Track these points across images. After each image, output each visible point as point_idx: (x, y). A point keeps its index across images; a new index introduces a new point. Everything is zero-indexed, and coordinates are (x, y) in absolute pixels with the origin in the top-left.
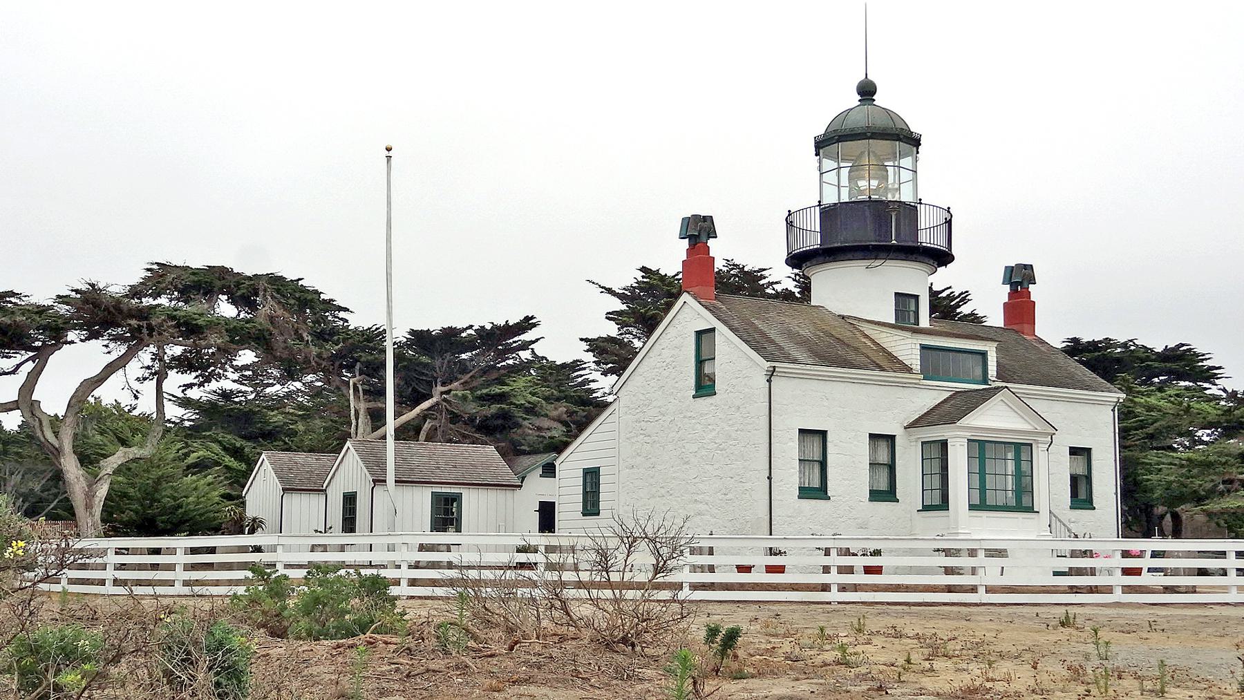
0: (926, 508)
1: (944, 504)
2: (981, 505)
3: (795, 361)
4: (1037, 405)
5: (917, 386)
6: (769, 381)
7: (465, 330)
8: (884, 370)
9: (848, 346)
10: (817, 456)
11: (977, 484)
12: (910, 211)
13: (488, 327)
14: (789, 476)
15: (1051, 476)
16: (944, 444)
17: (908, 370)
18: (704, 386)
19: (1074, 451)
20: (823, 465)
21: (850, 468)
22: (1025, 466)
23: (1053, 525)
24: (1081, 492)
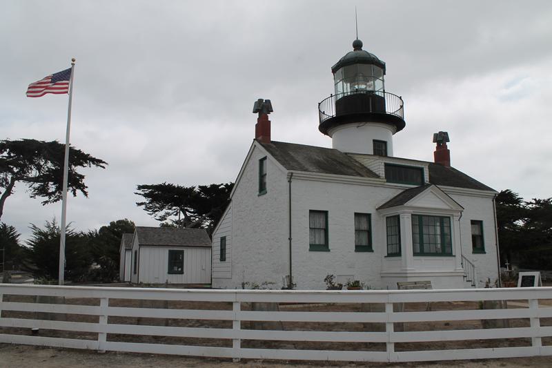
0: (389, 255)
1: (399, 254)
2: (420, 252)
3: (306, 170)
4: (452, 196)
5: (383, 186)
6: (290, 182)
7: (220, 185)
8: (362, 176)
9: (344, 165)
10: (323, 226)
11: (417, 231)
12: (381, 101)
13: (229, 184)
14: (303, 237)
15: (461, 236)
16: (398, 217)
17: (378, 177)
18: (262, 188)
19: (473, 222)
20: (326, 231)
21: (342, 232)
22: (446, 230)
23: (464, 263)
24: (478, 244)
